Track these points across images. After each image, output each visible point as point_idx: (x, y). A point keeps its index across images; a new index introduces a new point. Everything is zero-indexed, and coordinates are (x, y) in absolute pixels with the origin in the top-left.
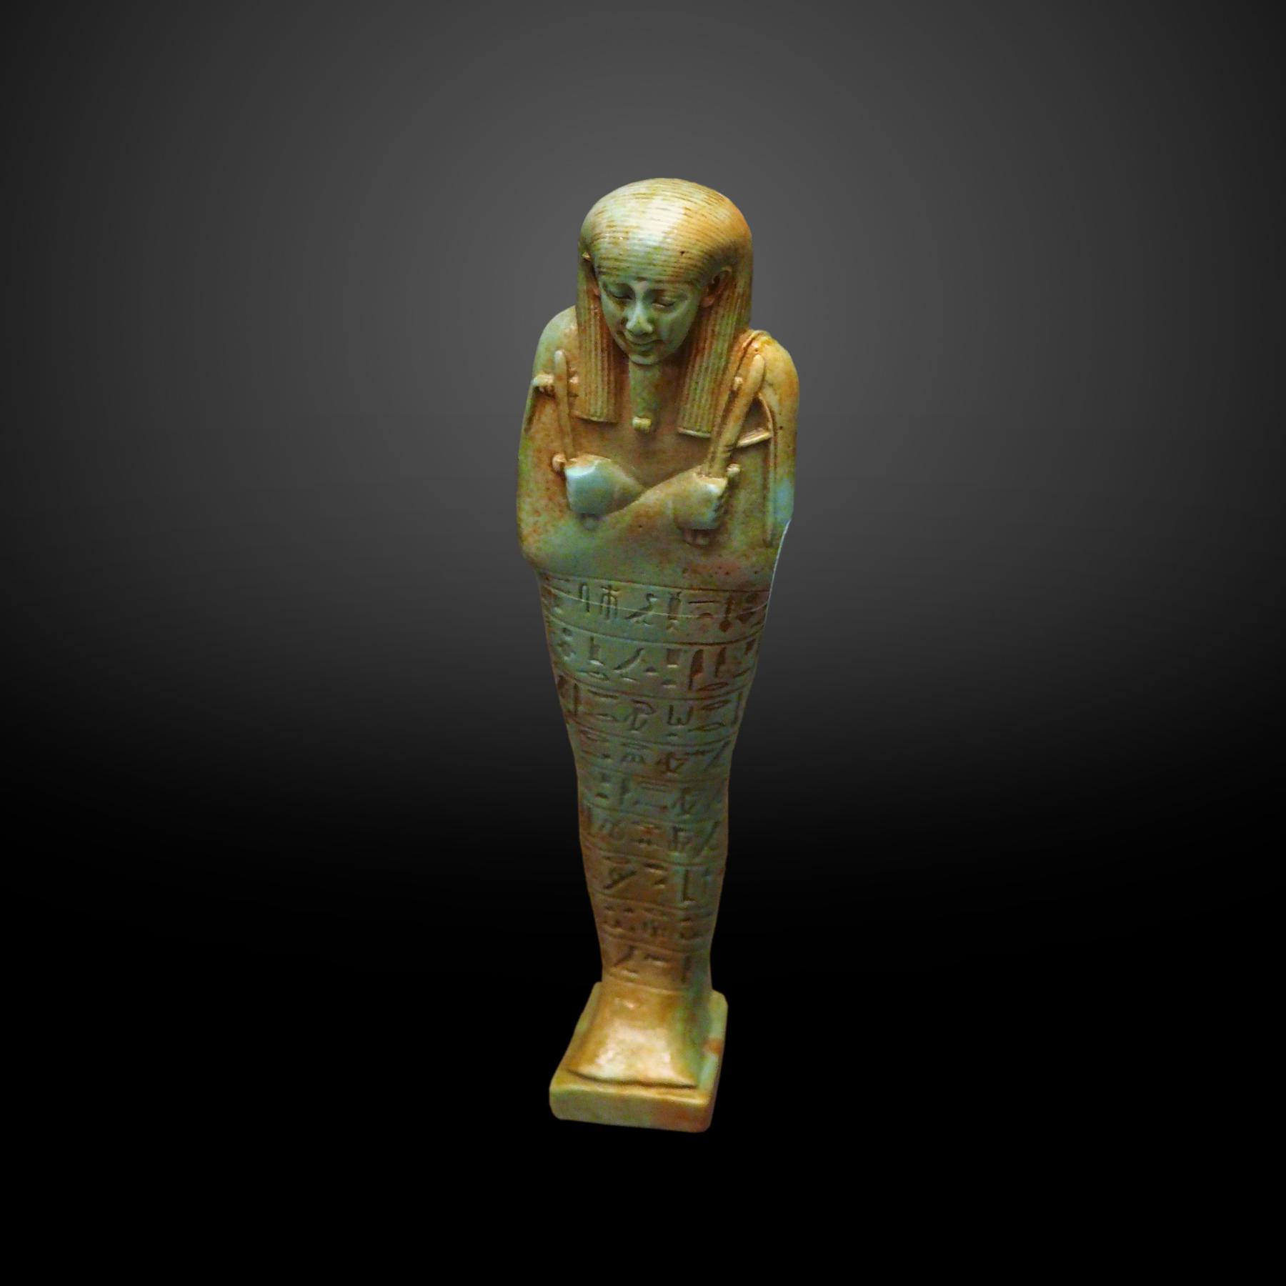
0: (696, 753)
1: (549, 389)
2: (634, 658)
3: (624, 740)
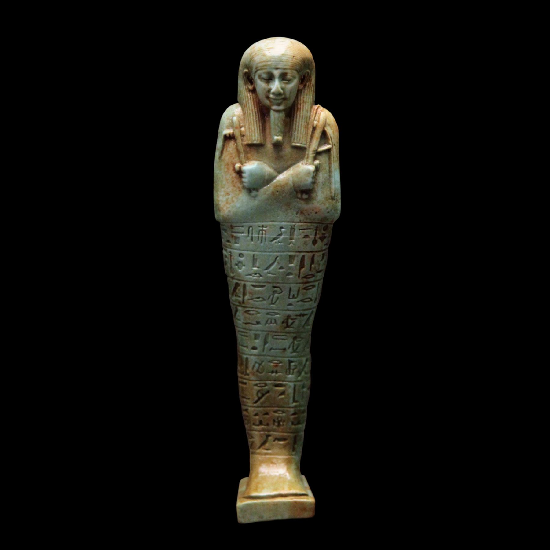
0: (300, 315)
1: (231, 134)
2: (273, 264)
3: (268, 311)
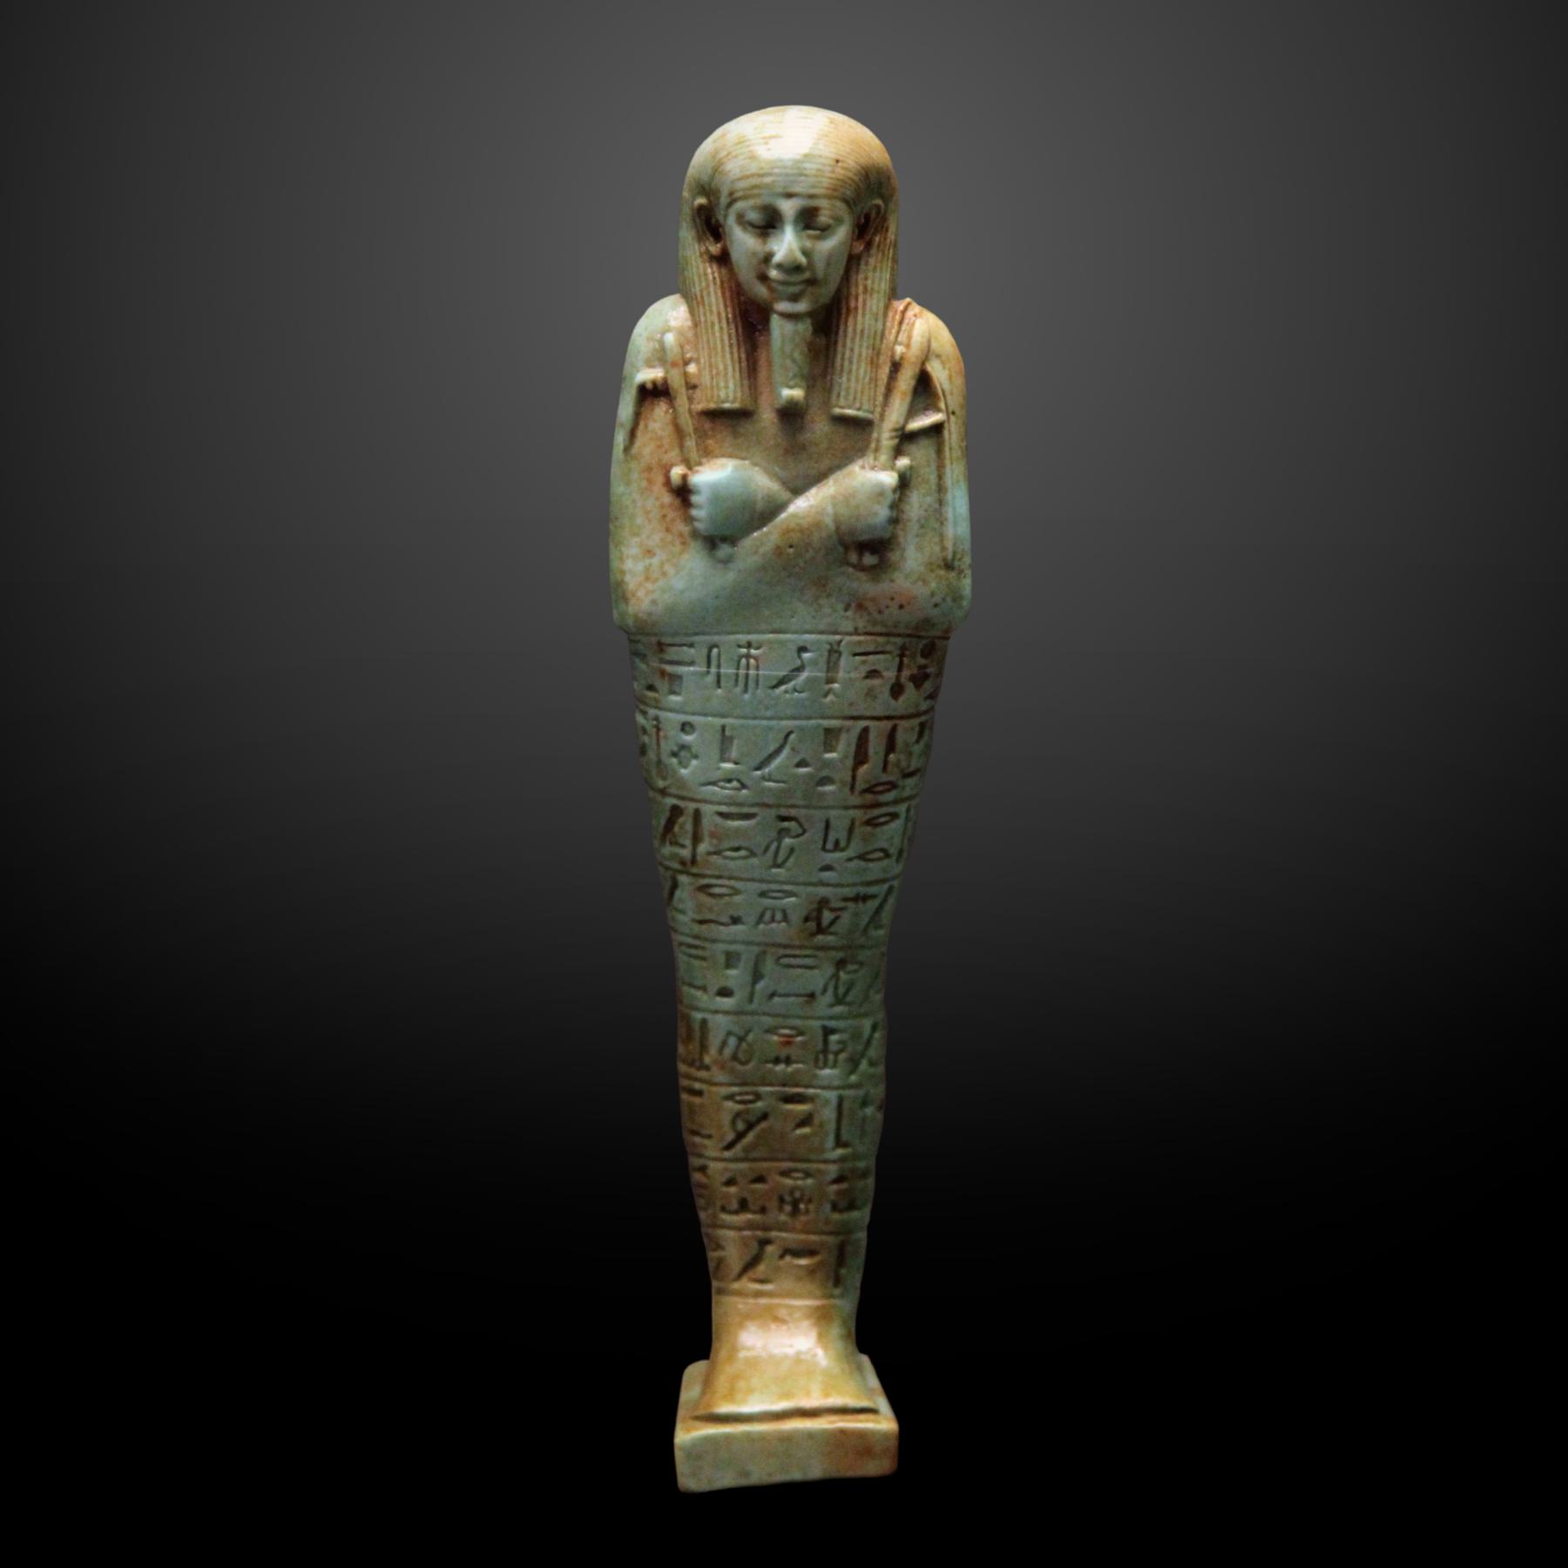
0: (856, 899)
1: (659, 383)
2: (778, 751)
3: (765, 887)
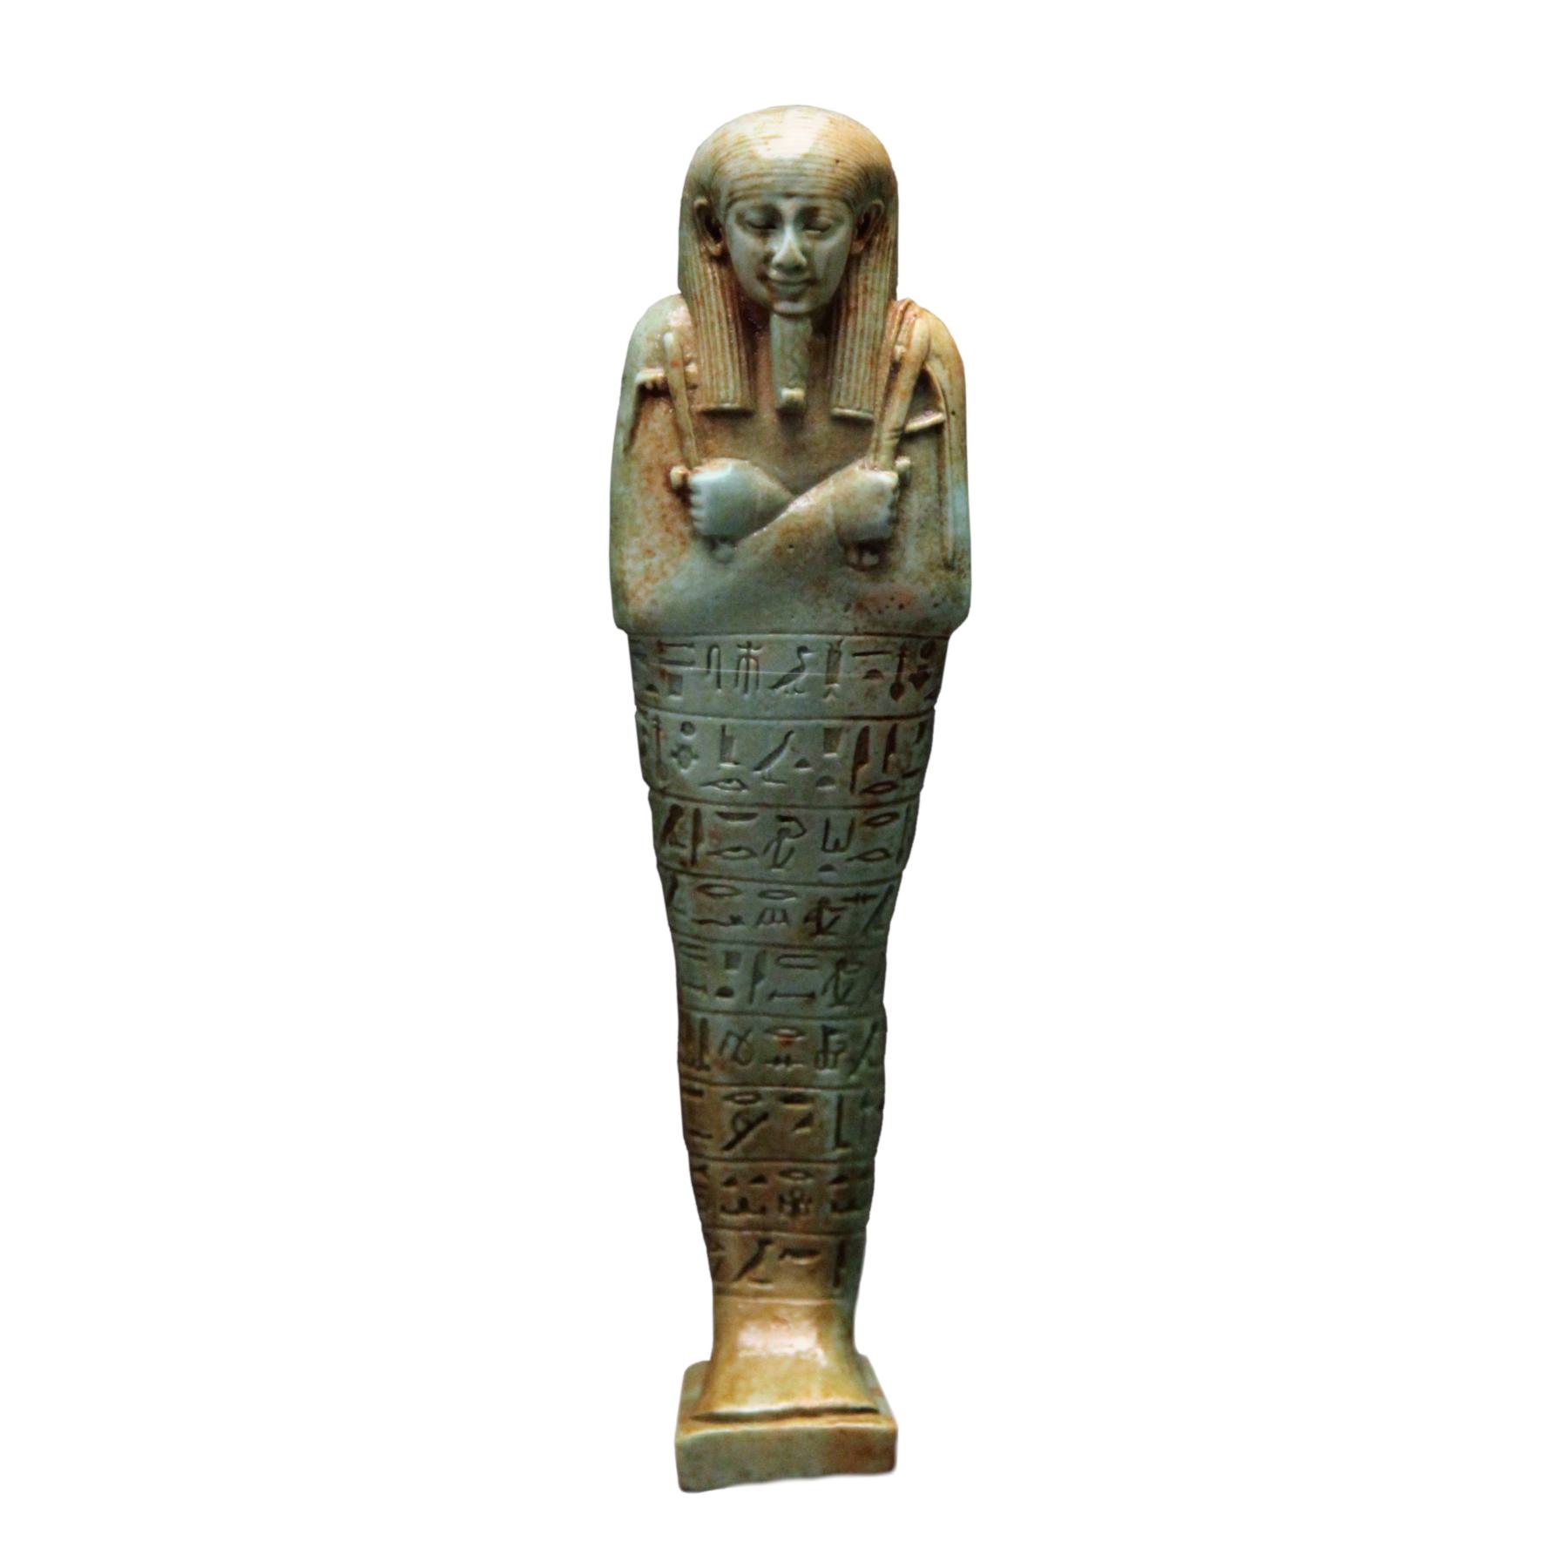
0: (856, 899)
1: (659, 383)
2: (778, 751)
3: (765, 887)
